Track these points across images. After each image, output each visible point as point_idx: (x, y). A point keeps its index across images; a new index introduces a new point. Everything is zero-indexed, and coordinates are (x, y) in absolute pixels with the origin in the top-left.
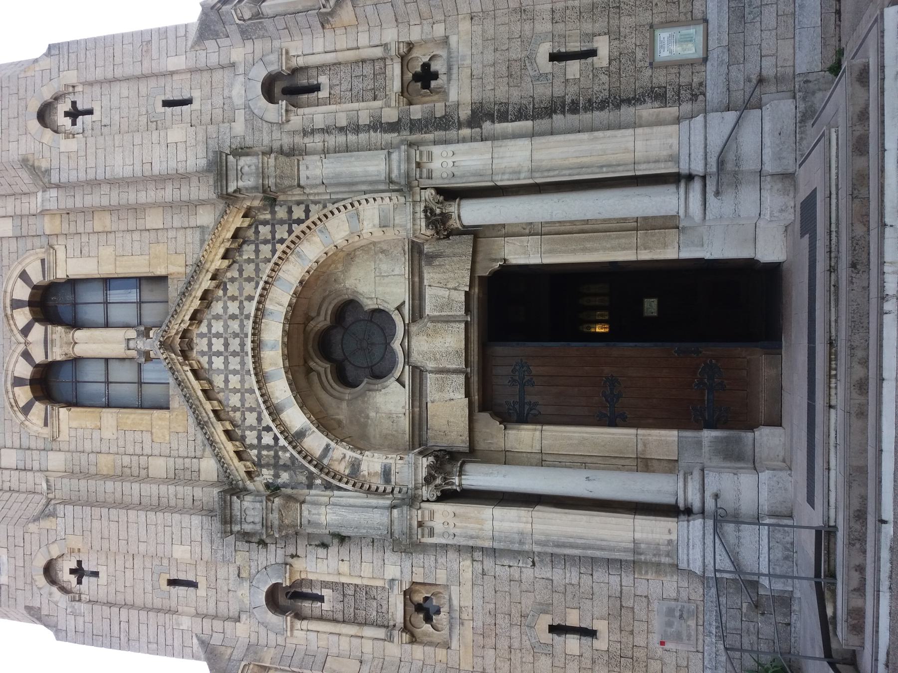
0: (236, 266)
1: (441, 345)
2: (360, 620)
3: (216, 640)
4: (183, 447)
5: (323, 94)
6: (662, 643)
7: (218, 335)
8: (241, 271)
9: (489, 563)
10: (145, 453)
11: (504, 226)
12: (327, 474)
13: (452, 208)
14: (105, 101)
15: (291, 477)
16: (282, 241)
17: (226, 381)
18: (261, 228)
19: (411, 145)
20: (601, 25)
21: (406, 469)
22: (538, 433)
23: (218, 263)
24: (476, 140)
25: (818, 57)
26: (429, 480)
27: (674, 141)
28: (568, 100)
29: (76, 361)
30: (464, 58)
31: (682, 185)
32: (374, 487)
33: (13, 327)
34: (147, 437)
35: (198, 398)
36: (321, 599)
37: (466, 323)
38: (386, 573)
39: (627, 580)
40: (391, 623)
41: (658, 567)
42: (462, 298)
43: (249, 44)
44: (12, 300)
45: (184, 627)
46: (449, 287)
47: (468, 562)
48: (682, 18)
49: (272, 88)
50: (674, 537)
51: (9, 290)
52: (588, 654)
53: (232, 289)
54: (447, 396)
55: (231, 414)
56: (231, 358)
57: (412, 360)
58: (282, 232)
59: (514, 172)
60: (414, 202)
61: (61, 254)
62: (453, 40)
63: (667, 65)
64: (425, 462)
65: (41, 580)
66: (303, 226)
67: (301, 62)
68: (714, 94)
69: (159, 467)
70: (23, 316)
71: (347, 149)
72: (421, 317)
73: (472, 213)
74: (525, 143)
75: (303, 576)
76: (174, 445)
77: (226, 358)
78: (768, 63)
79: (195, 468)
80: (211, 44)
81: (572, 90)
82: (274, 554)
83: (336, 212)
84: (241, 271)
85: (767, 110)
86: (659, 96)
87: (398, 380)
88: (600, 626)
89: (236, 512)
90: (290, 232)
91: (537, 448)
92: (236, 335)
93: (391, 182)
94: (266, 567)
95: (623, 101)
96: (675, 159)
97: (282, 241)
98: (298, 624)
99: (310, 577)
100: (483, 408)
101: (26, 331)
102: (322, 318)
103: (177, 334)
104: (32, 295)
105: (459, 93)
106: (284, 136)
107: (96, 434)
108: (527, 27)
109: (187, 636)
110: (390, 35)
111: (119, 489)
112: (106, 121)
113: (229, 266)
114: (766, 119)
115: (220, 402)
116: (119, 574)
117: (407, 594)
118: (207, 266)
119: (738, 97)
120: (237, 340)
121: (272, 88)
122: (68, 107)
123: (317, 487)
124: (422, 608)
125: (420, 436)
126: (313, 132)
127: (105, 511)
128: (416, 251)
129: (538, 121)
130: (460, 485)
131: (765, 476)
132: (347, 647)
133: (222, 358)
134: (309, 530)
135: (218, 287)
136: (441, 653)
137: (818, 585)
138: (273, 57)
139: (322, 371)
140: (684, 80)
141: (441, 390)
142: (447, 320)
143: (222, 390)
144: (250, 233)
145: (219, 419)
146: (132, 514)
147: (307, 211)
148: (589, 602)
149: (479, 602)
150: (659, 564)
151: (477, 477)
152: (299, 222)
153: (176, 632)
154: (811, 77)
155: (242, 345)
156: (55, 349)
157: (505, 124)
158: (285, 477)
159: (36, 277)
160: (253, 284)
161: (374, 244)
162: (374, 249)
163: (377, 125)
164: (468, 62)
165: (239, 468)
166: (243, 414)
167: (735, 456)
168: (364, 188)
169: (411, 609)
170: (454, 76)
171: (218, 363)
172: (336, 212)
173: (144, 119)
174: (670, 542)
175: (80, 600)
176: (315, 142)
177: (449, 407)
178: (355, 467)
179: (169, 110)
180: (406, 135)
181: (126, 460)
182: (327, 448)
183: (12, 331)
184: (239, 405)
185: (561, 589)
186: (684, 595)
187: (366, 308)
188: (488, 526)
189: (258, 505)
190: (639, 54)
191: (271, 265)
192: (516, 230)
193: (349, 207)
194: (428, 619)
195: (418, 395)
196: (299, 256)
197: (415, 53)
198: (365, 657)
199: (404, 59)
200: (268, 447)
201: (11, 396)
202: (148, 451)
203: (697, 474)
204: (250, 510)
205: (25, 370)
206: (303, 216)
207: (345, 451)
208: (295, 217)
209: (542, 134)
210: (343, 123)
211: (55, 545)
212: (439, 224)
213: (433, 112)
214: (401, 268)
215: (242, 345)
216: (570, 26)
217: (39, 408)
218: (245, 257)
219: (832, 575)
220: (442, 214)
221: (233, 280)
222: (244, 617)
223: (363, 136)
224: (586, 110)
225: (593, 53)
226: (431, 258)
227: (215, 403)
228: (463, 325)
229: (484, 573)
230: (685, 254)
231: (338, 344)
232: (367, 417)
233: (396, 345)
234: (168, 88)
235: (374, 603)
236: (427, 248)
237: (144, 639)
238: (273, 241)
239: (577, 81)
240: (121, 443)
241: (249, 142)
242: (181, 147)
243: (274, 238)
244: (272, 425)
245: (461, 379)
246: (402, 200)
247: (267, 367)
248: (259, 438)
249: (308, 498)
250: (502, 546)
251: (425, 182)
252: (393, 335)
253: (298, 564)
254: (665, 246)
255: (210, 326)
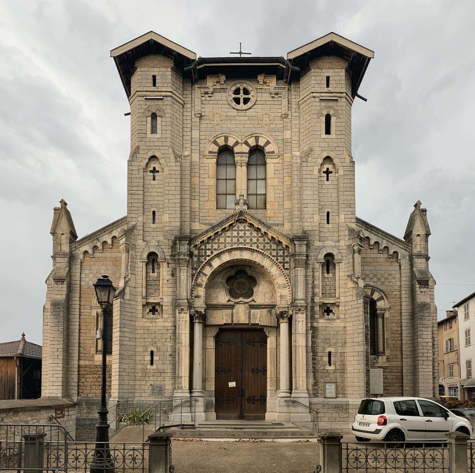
0: (269, 242)
1: (241, 315)
2: (148, 286)
3: (136, 232)
4: (203, 214)
5: (326, 275)
6: (151, 385)
7: (245, 234)
8: (267, 243)
9: (171, 331)
10: (200, 198)
11: (280, 336)
12: (197, 275)
13: (286, 320)
14: (331, 187)
15: (195, 261)
16: (277, 259)
17: (229, 237)
18: (282, 251)
19: (306, 307)
20: (338, 367)
21: (200, 304)
22: (212, 347)
23: (270, 235)
24: (306, 328)
25: (322, 428)
26: (197, 312)
27: (302, 388)
28: (316, 357)
29: (234, 165)
30: (332, 324)
31: (289, 391)
32: (193, 292)
33: (248, 137)
34: (206, 199)
35: (222, 226)
36: (153, 272)
37: (248, 324)
38: (164, 297)
39: (169, 374)
40: (148, 298)
41: (174, 384)
42: (257, 323)
43: (346, 247)
44: (258, 137)
45: (139, 219)
46: (260, 318)
47: (171, 325)
48: (338, 391)
49: (329, 256)
50: (184, 388)
51: (263, 136)
52: (145, 363)
53: (261, 240)
54: (224, 317)
55: (217, 239)
56: (237, 239)
57: (236, 305)
58: (280, 259)
59: (296, 341)
60: (288, 308)
61: (276, 161)
62: (338, 321)
63: (325, 386)
64: (203, 311)
65: (150, 154)
66: (282, 268)
67: (337, 267)
68: (315, 400)
69: (196, 204)
70: (252, 142)
71: (307, 284)
72: (251, 308)
73: (284, 327)
74: (304, 344)
75: (161, 266)
76: (204, 211)
77: (237, 237)
78: (322, 415)
79: (196, 220)
80: (347, 233)
81: (319, 359)
82: (168, 252)
83: (286, 280)
84: (267, 243)
85: (309, 414)
86: (315, 384)
87: (229, 300)
88: (154, 366)
89: (183, 242)
90: (280, 263)
91: (207, 347)
92: (245, 241)
93: (295, 300)
94: (164, 252)
95: (315, 374)
96: (296, 389)
97: (277, 259)
98: (144, 264)
99: (161, 269)
100: (220, 329)
101: (246, 143)
102: (251, 272)
103: (246, 218)
104: (260, 146)
105: (321, 323)
106: (313, 261)
107: (207, 176)
108: (340, 345)
109: (136, 220)
110: (342, 299)
111: (187, 189)
112: (324, 186)
113: (269, 239)
114: (306, 414)
115: (221, 234)
116: (155, 190)
117: (158, 304)
118: (269, 231)
119: (313, 407)
120: (243, 241)
121: (329, 256)
122: (330, 170)
123: (192, 271)
124: (154, 309)
125: (210, 307)
126: (313, 272)
127: (179, 184)
128: (272, 306)
129: (311, 348)
130: (195, 322)
131: (203, 414)
132: (138, 282)
133: (236, 235)
134: (178, 269)
135: (262, 234)
136: (140, 315)
137: (180, 425)
138: (340, 257)
139: (232, 272)
140: (319, 391)
141: (226, 315)
142: (249, 317)
143: (225, 235)
144: (280, 247)
145: (215, 234)
146: (179, 197)
147: (287, 269)
148: (161, 363)
149: (158, 328)
150: (175, 384)
151: (198, 328)
152: (284, 266)
153: (136, 215)
154: (317, 426)
155: (241, 243)
156: (239, 157)
157: (311, 337)
158: (195, 259)
159: (267, 149)
160: (263, 248)
161: (276, 292)
162: (273, 292)
163: (314, 294)
164: (331, 326)
165: (198, 242)
166: (217, 243)
167: (207, 407)
168: (294, 290)
169: (153, 305)
170: (327, 321)
171: (235, 234)
172: (286, 280)
173: (323, 203)
174: (182, 387)
175: (144, 172)
176: (310, 273)
177: (221, 318)
178: (200, 285)
179: (326, 214)
180: (310, 304)
181: (197, 190)
182: (206, 275)
183: (247, 137)
184: (220, 241)
185: (165, 355)
186: (166, 391)
187: (254, 288)
188: (183, 332)
189: (186, 251)
190: (328, 378)
191: (269, 255)
192: (278, 338)
193: (288, 284)
194: (150, 311)
195: (224, 307)
196: (272, 265)
197: (336, 308)
198: (136, 289)
199: (333, 304)
200: (206, 253)
201: (221, 135)
202: (201, 199)
203: (202, 395)
204: (184, 248)
205: (231, 143)
206: (285, 267)
207: (205, 282)
208: (285, 264)
209: (307, 349)
210: (315, 283)
211: (164, 161)
212: (282, 315)
213: (316, 314)
214: (267, 301)
215: (241, 243)
216: (339, 358)
217: (216, 149)
218: (272, 245)
219: (183, 428)
220: (284, 317)
221: (264, 240)
222: (145, 243)
223: (310, 290)
224: (313, 363)
225: (330, 365)
226: (270, 312)
227: (221, 232)
228: (248, 323)
229: (167, 330)
230: (268, 392)
231: (241, 277)
232: (216, 289)
233: (241, 299)
234: (334, 214)
235: (154, 292)
236: (273, 310)
237: (132, 201)
238: (277, 256)
239: (322, 360)
240: (203, 187)
241: (311, 247)
242: (312, 220)
243: (279, 256)
244: (213, 255)
245: (230, 322)
246: (289, 303)
247: (234, 253)
248: (209, 249)
249: (189, 268)
250: (177, 336)
251: (294, 311)
252: (244, 298)
253: (165, 265)
254: (271, 386)
255: (248, 230)
